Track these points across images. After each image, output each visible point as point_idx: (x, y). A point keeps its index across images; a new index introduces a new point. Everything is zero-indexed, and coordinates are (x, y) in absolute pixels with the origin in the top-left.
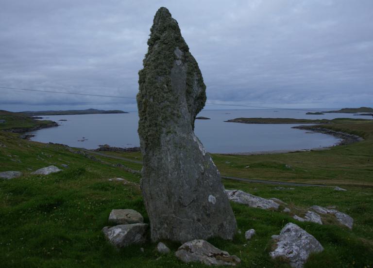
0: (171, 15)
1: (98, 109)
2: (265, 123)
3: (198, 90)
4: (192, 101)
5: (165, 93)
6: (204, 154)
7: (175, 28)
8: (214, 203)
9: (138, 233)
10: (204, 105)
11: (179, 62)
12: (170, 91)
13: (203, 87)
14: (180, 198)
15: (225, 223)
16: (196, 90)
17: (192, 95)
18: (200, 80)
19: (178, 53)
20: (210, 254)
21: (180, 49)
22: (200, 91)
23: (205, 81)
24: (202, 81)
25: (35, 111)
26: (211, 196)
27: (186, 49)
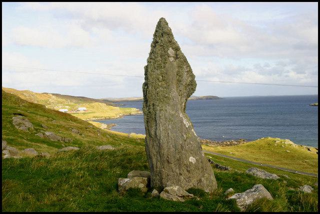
0: (167, 24)
1: (220, 95)
2: (109, 100)
3: (188, 78)
4: (182, 88)
5: (160, 81)
6: (187, 127)
7: (169, 34)
8: (194, 163)
9: (141, 183)
10: (194, 90)
11: (172, 59)
12: (163, 80)
13: (193, 76)
14: (168, 157)
15: (203, 179)
16: (186, 79)
17: (181, 83)
18: (190, 71)
19: (171, 51)
20: (180, 195)
21: (173, 49)
22: (190, 79)
23: (195, 72)
24: (192, 72)
25: (130, 97)
26: (191, 158)
27: (177, 49)
